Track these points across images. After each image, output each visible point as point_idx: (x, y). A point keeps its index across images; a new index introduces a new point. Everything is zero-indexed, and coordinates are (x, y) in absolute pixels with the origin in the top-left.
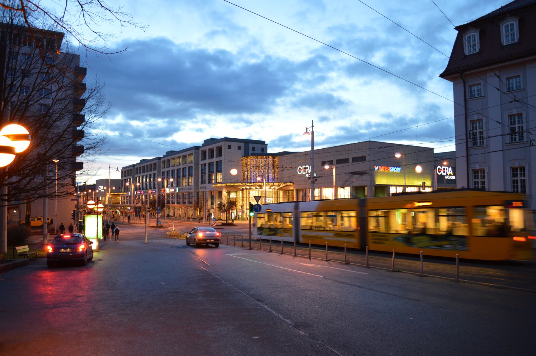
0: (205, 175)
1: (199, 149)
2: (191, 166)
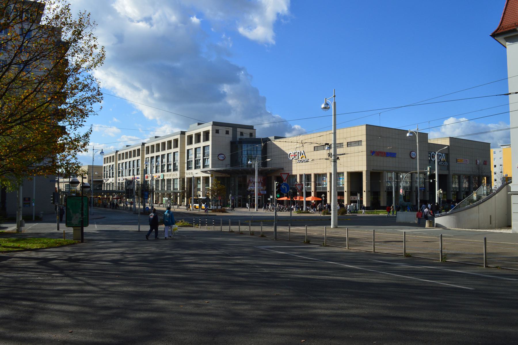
0: (208, 159)
1: (185, 134)
2: (199, 148)
